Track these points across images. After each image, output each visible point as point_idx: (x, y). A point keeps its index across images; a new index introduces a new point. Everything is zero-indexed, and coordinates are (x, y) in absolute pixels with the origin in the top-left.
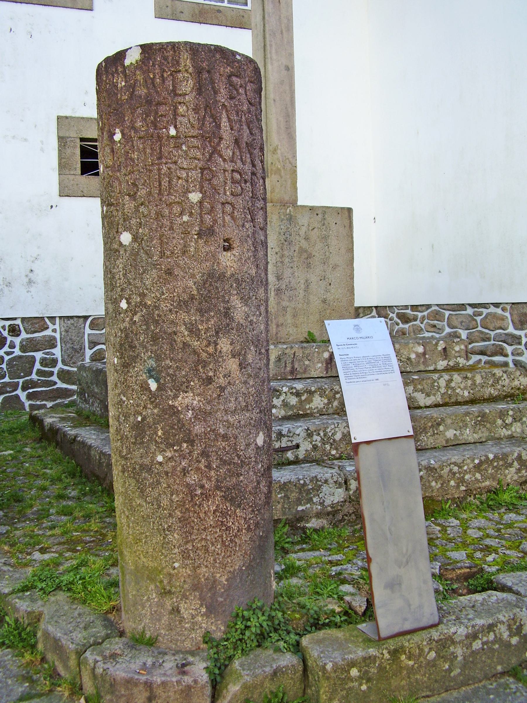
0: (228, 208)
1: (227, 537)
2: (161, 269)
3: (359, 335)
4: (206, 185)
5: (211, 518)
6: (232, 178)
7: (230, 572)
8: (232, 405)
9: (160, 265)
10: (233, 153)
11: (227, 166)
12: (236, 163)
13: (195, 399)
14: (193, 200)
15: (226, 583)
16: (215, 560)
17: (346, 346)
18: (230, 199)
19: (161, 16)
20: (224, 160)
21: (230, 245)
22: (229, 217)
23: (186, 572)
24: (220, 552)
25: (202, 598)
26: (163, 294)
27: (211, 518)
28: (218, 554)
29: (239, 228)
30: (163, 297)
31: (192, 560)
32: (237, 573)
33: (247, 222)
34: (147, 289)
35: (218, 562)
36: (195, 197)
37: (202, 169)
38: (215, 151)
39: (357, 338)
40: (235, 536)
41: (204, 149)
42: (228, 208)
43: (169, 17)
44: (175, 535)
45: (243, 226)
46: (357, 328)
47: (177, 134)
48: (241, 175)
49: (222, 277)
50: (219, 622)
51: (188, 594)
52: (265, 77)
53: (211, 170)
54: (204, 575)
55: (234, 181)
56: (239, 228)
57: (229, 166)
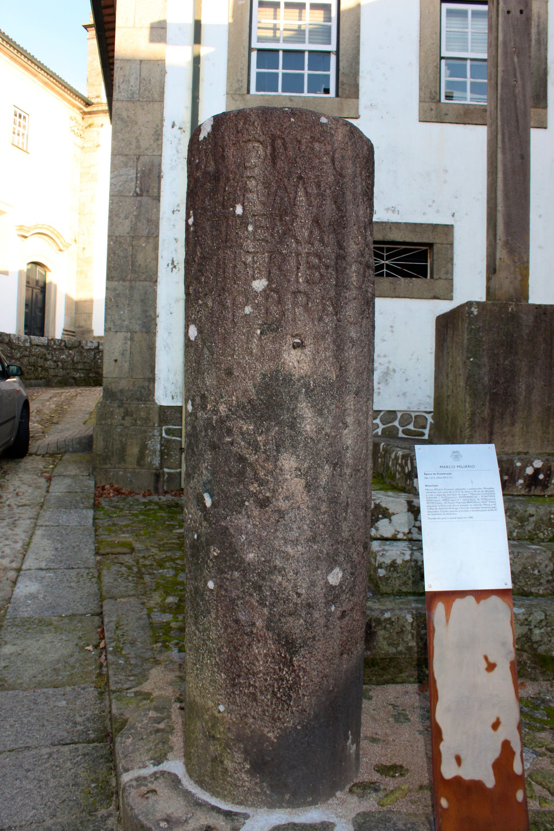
0: (301, 299)
1: (279, 688)
2: (220, 369)
3: (456, 464)
4: (274, 270)
5: (261, 663)
6: (308, 262)
7: (281, 729)
8: (294, 534)
9: (220, 364)
10: (311, 233)
11: (300, 248)
12: (313, 244)
13: (249, 523)
14: (256, 289)
15: (275, 740)
16: (263, 711)
17: (436, 476)
18: (303, 287)
19: (425, 120)
20: (298, 242)
21: (302, 342)
22: (301, 308)
23: (231, 719)
24: (269, 703)
25: (246, 752)
26: (222, 398)
27: (261, 663)
28: (267, 706)
29: (313, 322)
30: (222, 400)
31: (238, 706)
32: (290, 732)
33: (327, 315)
34: (207, 390)
35: (267, 714)
36: (259, 285)
37: (271, 252)
38: (288, 232)
39: (454, 467)
40: (290, 689)
41: (273, 229)
42: (301, 299)
43: (433, 120)
44: (223, 675)
45: (320, 319)
46: (456, 456)
47: (243, 213)
48: (320, 259)
49: (288, 380)
50: (264, 784)
51: (231, 744)
52: (61, 95)
53: (281, 253)
54: (250, 726)
55: (311, 267)
56: (313, 322)
57: (305, 249)
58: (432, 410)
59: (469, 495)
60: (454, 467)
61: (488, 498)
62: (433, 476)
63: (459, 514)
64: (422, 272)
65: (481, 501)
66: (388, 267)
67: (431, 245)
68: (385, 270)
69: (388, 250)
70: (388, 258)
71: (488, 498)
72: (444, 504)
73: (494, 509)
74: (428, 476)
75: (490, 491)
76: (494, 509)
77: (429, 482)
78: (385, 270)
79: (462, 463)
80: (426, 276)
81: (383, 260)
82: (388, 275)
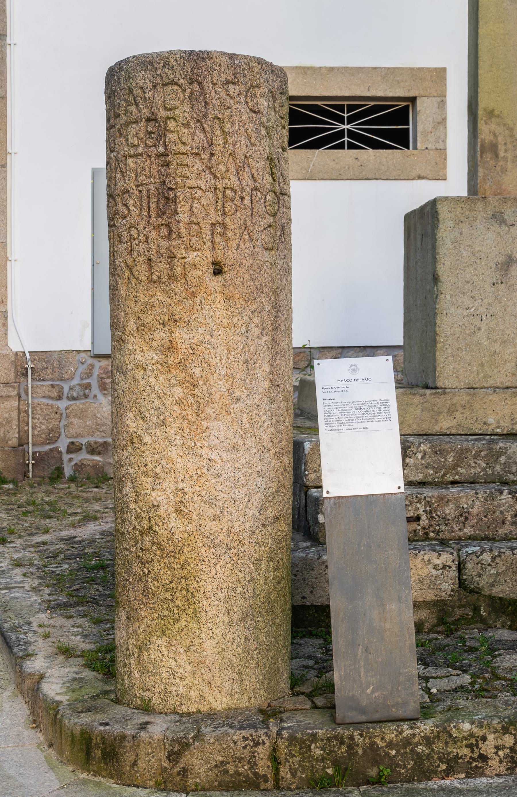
3: (353, 377)
17: (334, 390)
39: (351, 380)
46: (354, 369)
58: (400, 341)
59: (364, 407)
60: (351, 380)
61: (383, 409)
62: (331, 390)
63: (355, 426)
64: (402, 139)
65: (376, 412)
66: (351, 134)
67: (413, 100)
68: (346, 139)
69: (351, 108)
70: (351, 120)
71: (383, 409)
72: (341, 417)
73: (389, 419)
74: (325, 390)
75: (386, 404)
76: (389, 419)
77: (326, 396)
78: (346, 139)
79: (359, 376)
80: (408, 148)
81: (344, 124)
82: (351, 146)
